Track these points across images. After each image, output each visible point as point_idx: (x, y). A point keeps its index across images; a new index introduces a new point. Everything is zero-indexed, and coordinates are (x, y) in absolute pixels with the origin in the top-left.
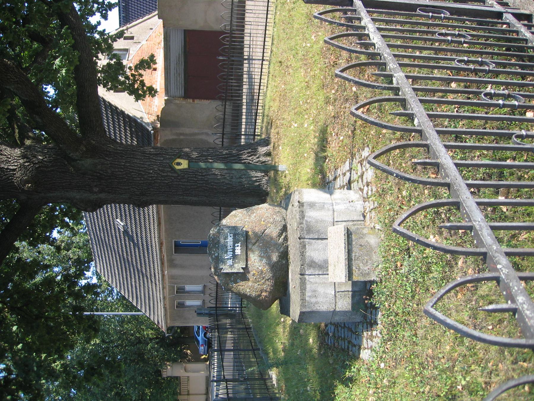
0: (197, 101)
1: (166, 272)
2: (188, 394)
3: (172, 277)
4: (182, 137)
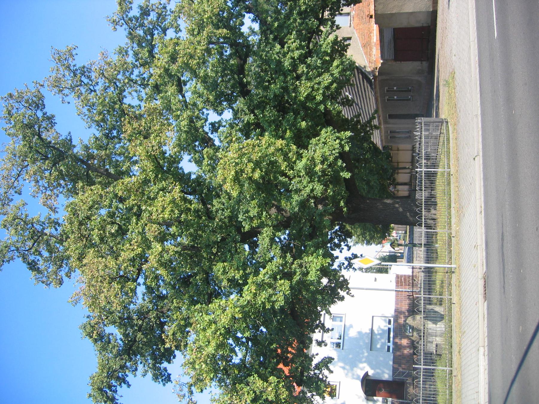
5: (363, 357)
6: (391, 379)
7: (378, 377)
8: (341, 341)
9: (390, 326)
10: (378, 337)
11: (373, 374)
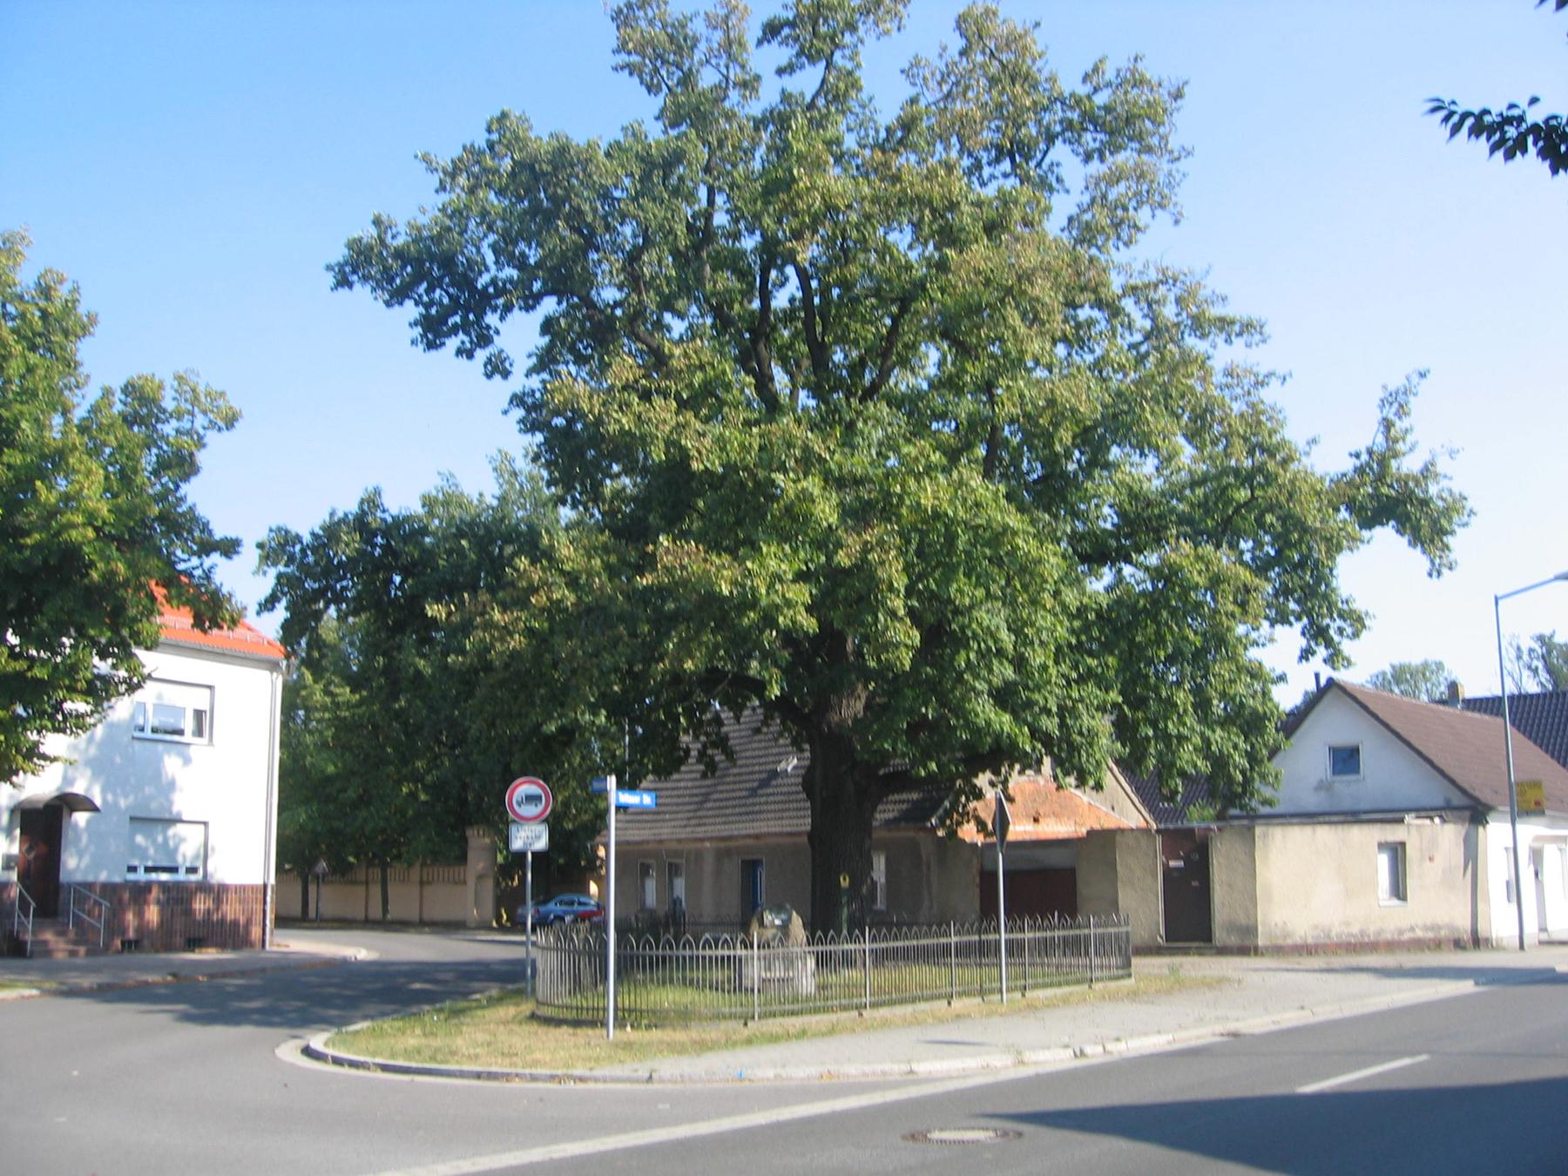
0: (977, 891)
1: (708, 844)
2: (422, 883)
3: (699, 855)
5: (115, 795)
6: (63, 877)
7: (68, 836)
8: (148, 734)
9: (182, 871)
10: (160, 839)
11: (76, 825)
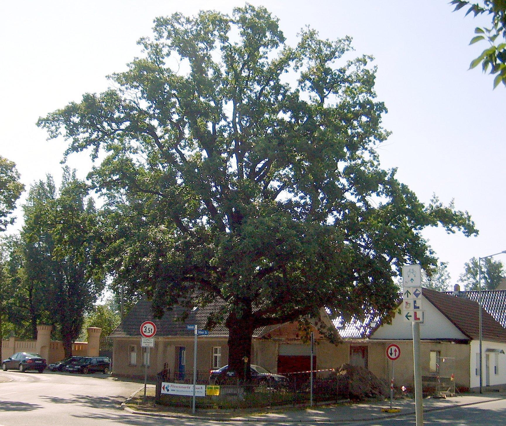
4: (255, 354)
